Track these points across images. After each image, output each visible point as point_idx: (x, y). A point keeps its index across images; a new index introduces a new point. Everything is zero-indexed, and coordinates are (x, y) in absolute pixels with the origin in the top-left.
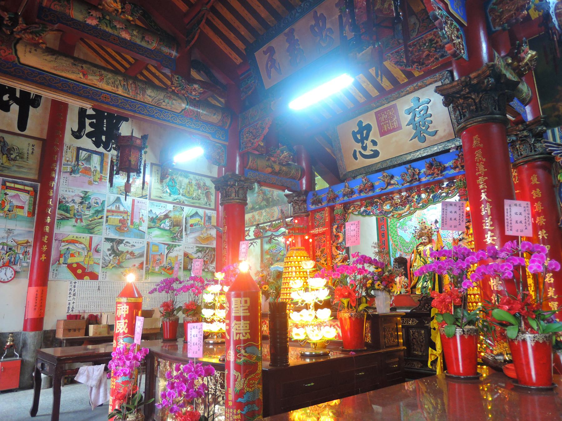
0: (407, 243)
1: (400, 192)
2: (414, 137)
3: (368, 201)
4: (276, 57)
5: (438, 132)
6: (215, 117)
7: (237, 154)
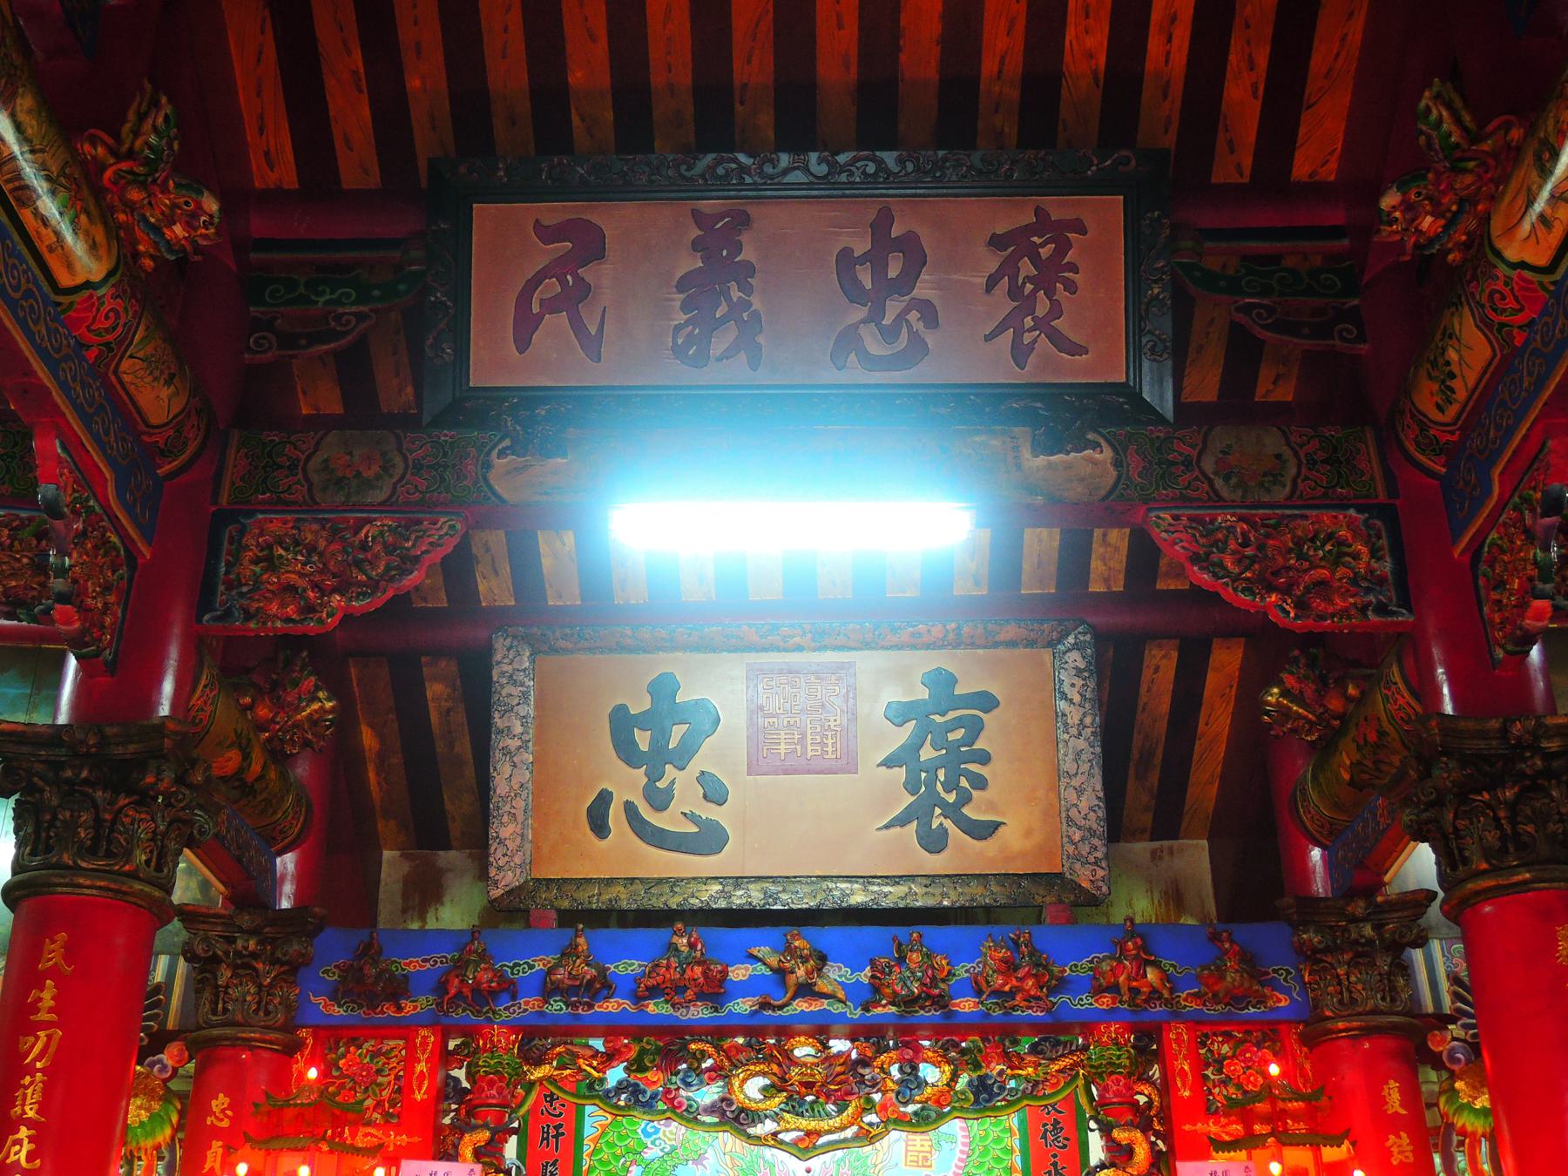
1: (821, 1032)
2: (901, 821)
3: (650, 1043)
4: (600, 275)
5: (1001, 829)
6: (165, 392)
7: (177, 631)
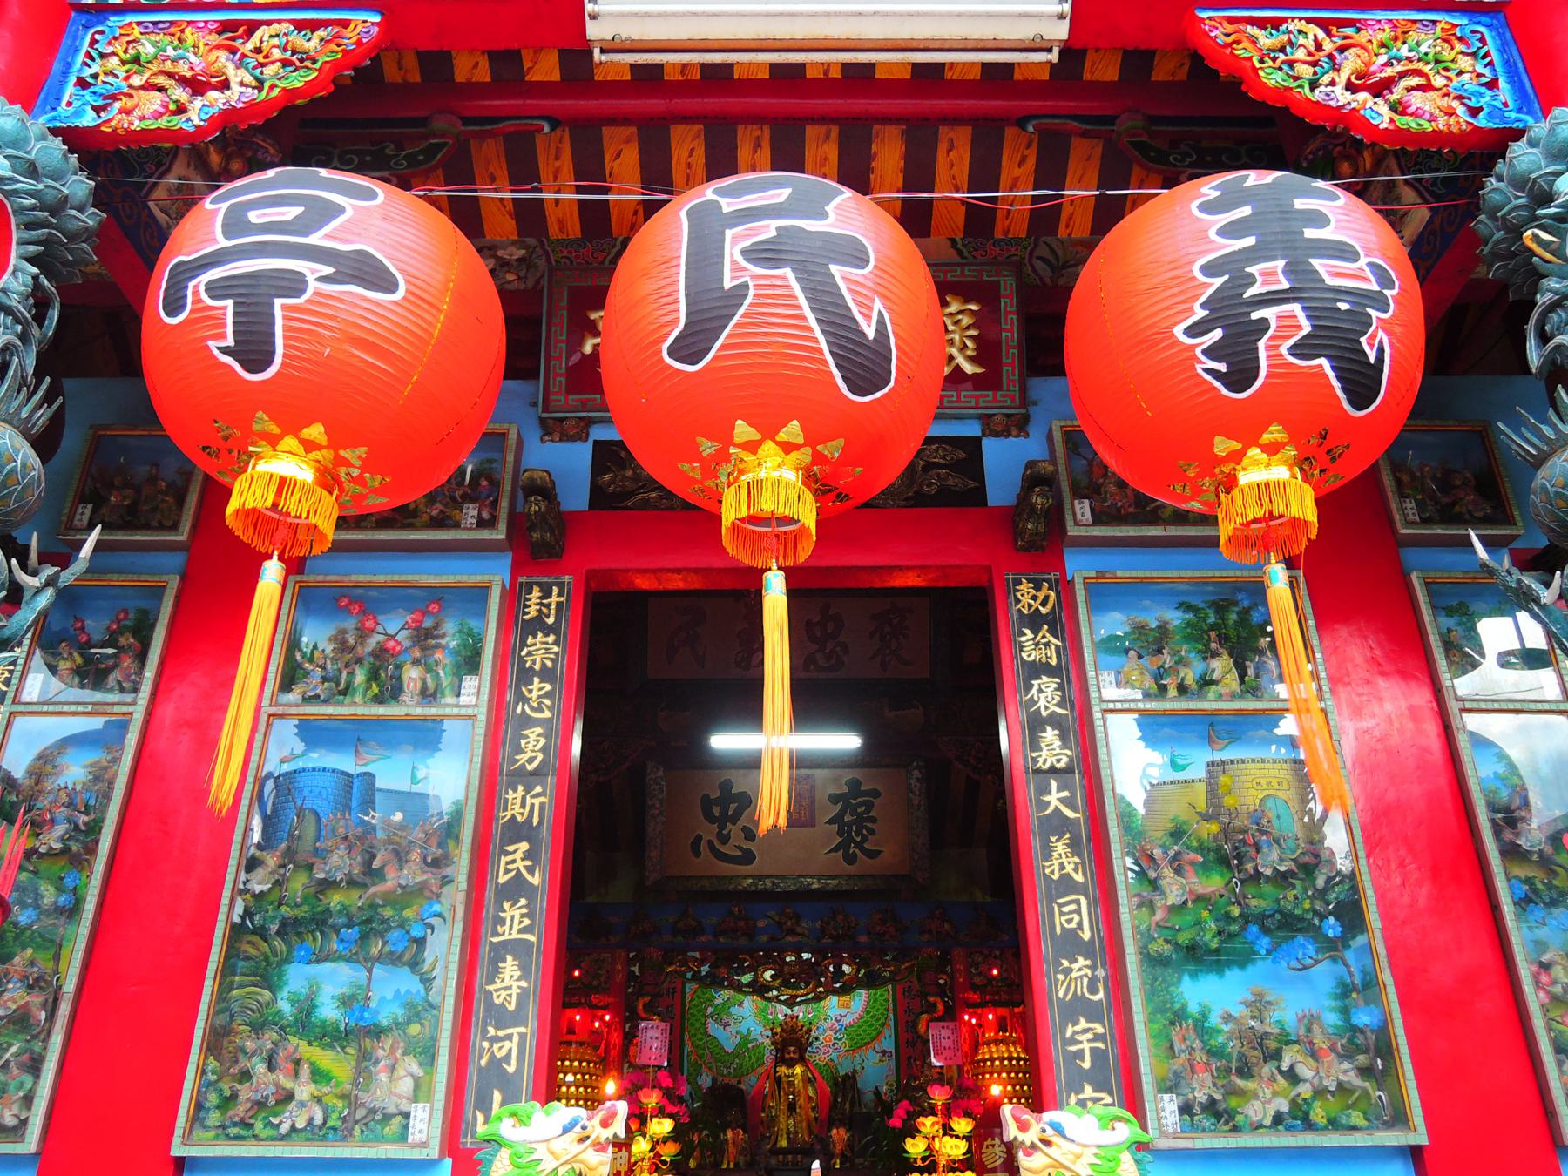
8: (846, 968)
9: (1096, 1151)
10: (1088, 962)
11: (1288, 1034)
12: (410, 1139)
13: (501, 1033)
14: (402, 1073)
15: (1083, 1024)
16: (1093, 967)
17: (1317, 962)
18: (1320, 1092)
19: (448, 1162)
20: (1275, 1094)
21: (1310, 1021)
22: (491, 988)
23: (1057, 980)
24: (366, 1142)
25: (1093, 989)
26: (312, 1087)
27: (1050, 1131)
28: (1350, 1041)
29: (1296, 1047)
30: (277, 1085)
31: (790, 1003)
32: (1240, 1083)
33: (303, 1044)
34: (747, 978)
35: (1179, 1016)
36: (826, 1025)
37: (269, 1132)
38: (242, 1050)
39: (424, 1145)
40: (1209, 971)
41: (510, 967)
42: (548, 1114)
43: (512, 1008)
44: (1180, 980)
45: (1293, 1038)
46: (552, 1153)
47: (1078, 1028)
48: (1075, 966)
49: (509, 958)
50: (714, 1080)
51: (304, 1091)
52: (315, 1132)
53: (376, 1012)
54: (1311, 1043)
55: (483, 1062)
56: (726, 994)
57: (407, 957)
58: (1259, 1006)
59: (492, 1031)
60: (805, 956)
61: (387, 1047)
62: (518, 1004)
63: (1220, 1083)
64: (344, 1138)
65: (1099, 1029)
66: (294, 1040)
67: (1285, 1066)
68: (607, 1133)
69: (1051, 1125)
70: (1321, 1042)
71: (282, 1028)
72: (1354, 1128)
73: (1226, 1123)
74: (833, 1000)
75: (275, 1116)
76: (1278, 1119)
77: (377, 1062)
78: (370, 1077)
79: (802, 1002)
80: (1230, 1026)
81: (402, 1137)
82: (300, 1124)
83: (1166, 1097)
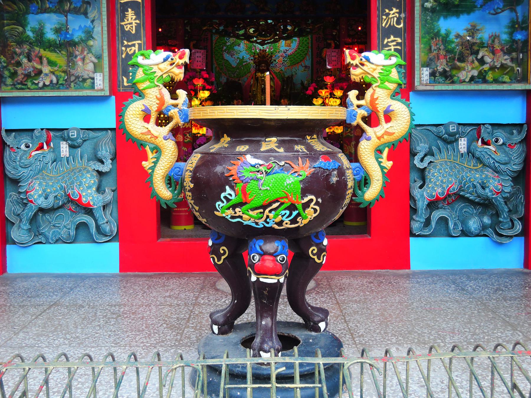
0: (233, 68)
8: (289, 28)
9: (382, 67)
10: (397, 11)
11: (483, 43)
12: (96, 88)
13: (130, 44)
14: (88, 61)
15: (392, 38)
16: (399, 13)
17: (503, 11)
18: (492, 68)
19: (113, 98)
20: (473, 68)
21: (494, 37)
22: (123, 23)
23: (382, 18)
24: (76, 89)
25: (398, 23)
26: (49, 68)
27: (364, 60)
28: (511, 46)
29: (486, 49)
30: (34, 67)
31: (262, 44)
32: (458, 64)
33: (42, 50)
34: (242, 32)
35: (437, 34)
36: (279, 55)
37: (33, 87)
38: (15, 53)
39: (102, 90)
40: (453, 15)
41: (130, 14)
42: (157, 55)
43: (134, 32)
44: (438, 19)
45: (485, 45)
46: (160, 69)
47: (389, 40)
48: (392, 12)
49: (130, 10)
50: (227, 79)
51: (46, 69)
52: (53, 86)
53: (72, 35)
54: (493, 47)
55: (123, 56)
56: (232, 40)
57: (82, 10)
58: (473, 31)
59: (126, 43)
60: (269, 21)
61: (80, 50)
62: (136, 30)
63: (449, 64)
64: (67, 88)
65: (399, 40)
66: (37, 49)
67: (479, 57)
68: (181, 62)
69: (365, 57)
70: (497, 47)
71: (31, 43)
72: (504, 83)
73: (449, 80)
74: (283, 43)
75: (36, 80)
76: (472, 79)
77: (76, 57)
78: (74, 64)
79: (268, 43)
80: (458, 40)
81: (92, 87)
82: (47, 83)
83: (425, 69)
